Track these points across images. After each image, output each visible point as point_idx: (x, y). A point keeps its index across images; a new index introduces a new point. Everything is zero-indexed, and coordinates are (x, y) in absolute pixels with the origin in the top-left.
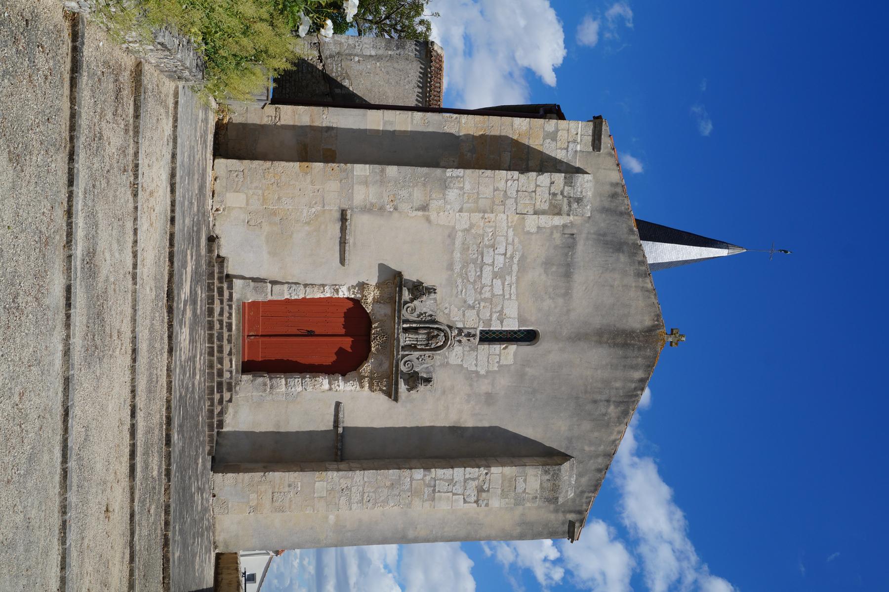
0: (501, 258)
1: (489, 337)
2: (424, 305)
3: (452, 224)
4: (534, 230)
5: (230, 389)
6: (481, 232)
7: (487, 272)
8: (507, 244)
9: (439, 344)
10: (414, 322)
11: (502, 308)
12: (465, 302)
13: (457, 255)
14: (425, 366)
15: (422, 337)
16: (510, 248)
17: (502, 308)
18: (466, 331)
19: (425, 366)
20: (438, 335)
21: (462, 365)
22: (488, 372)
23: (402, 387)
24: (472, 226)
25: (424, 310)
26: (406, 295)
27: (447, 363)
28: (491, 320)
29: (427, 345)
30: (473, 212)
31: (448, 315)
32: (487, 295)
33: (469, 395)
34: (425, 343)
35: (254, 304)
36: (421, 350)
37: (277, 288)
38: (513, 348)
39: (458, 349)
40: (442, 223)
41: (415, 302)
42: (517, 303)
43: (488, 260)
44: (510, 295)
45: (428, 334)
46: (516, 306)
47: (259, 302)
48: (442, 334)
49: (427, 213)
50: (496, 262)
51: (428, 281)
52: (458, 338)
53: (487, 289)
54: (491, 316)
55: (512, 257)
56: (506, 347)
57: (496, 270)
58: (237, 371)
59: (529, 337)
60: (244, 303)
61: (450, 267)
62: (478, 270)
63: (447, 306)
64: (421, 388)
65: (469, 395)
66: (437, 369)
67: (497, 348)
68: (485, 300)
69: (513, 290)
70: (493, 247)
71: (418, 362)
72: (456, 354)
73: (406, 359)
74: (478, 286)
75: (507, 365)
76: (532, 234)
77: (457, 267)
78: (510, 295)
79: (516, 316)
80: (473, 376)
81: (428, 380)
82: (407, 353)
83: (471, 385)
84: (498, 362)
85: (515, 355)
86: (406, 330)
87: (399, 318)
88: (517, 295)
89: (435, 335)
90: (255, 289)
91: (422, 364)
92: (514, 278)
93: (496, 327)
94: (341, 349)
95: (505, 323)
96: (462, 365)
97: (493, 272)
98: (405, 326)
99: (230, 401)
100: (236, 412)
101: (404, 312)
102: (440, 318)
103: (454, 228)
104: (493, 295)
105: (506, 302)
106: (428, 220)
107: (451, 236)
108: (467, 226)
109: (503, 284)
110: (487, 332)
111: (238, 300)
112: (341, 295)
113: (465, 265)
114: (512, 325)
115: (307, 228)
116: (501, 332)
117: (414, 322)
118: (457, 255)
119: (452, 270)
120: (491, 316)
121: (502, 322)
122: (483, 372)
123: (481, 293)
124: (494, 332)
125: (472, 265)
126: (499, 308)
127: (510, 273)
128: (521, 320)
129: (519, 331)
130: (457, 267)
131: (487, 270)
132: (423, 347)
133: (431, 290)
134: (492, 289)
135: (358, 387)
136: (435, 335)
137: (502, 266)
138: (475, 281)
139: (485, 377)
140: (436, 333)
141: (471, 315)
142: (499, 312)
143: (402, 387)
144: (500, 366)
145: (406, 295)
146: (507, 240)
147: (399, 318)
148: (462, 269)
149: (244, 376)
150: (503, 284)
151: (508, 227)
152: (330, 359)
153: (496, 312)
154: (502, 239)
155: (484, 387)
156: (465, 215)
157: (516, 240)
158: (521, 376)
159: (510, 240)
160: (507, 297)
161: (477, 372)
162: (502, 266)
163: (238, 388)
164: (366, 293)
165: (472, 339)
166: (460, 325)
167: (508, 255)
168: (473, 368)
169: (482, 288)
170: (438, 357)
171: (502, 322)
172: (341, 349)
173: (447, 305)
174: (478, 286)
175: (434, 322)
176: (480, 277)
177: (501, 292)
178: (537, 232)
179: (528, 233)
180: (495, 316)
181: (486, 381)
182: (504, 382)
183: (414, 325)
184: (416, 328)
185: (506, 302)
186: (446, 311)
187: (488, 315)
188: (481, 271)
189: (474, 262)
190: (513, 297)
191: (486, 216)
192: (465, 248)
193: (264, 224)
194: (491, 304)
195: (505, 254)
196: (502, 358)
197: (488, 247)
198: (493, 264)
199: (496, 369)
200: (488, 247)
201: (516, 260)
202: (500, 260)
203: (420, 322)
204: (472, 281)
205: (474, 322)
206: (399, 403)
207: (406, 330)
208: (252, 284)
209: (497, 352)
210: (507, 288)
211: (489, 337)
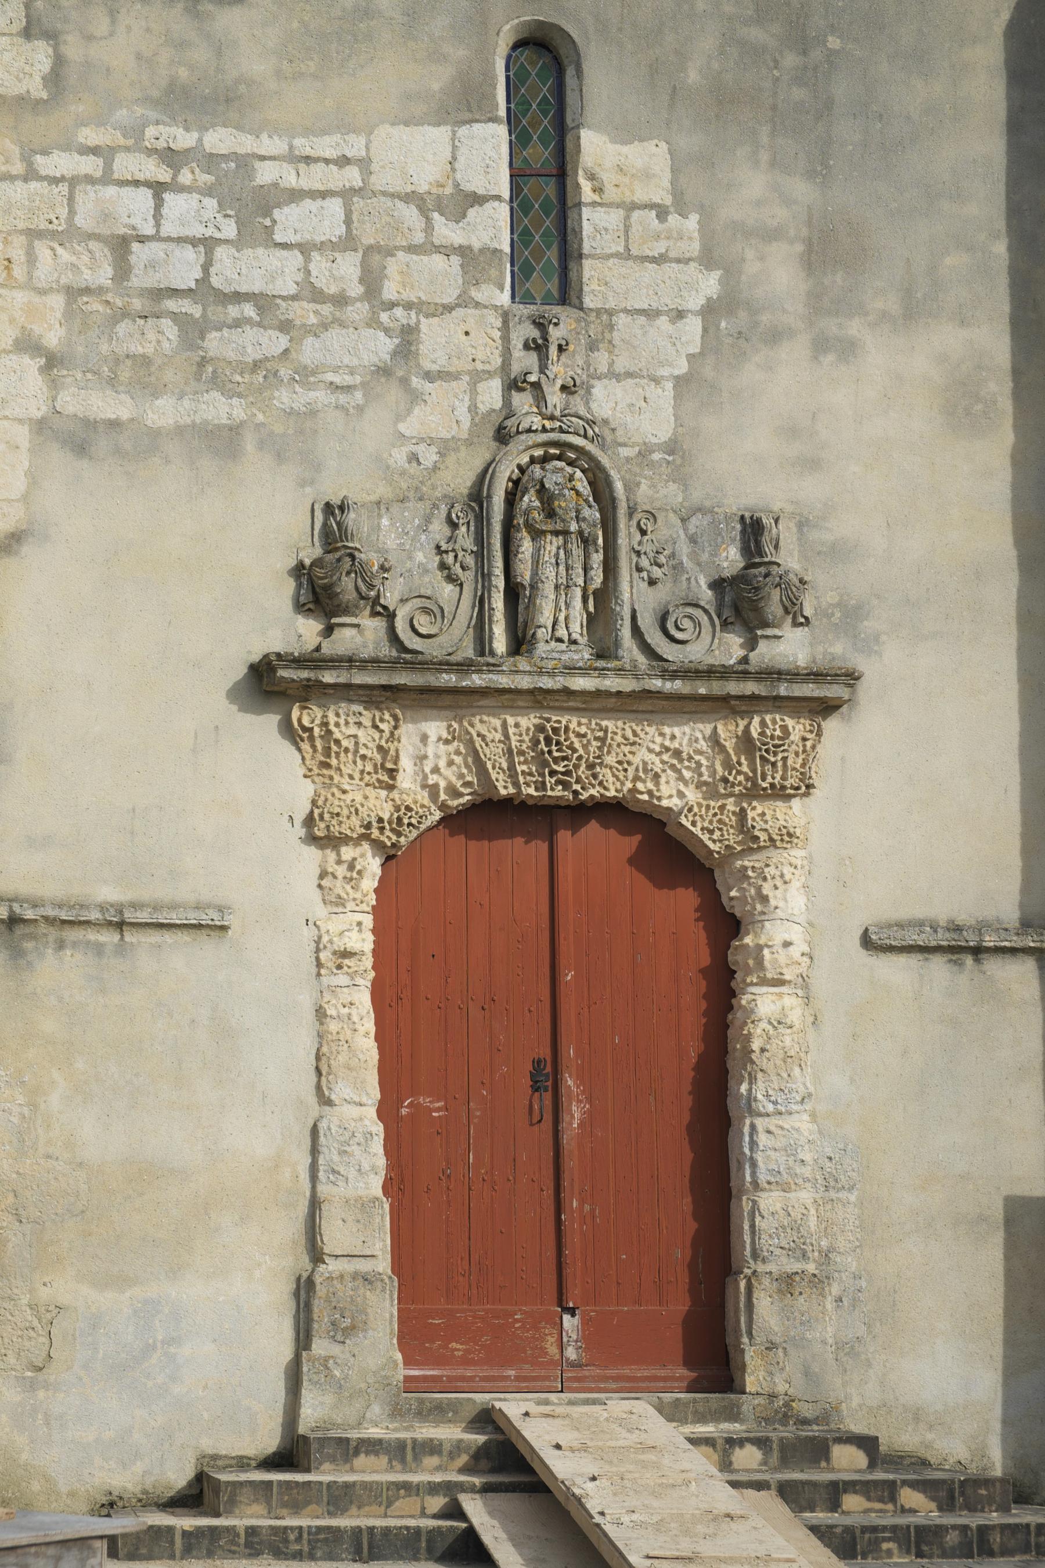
0: (175, 204)
1: (549, 233)
2: (406, 551)
3: (22, 435)
4: (41, 56)
5: (817, 1450)
6: (57, 302)
7: (240, 269)
8: (107, 179)
9: (582, 485)
10: (482, 602)
11: (408, 198)
12: (383, 371)
13: (164, 412)
14: (684, 550)
15: (542, 559)
16: (127, 165)
17: (408, 198)
18: (524, 361)
19: (684, 550)
21: (680, 382)
22: (708, 260)
23: (789, 647)
25: (424, 557)
26: (361, 635)
27: (672, 447)
28: (463, 251)
29: (586, 541)
32: (348, 269)
34: (577, 552)
35: (413, 1336)
36: (610, 567)
37: (336, 1235)
38: (595, 147)
39: (606, 401)
41: (390, 598)
42: (384, 131)
43: (184, 267)
44: (343, 161)
46: (401, 133)
47: (404, 1318)
48: (537, 470)
50: (198, 231)
53: (319, 264)
54: (446, 250)
55: (171, 157)
56: (592, 177)
57: (230, 230)
58: (732, 1414)
59: (545, 59)
60: (857, 679)
61: (223, 442)
62: (233, 311)
63: (407, 444)
64: (789, 558)
65: (821, 345)
66: (697, 495)
67: (597, 225)
68: (371, 282)
69: (327, 146)
70: (121, 246)
71: (668, 577)
72: (631, 410)
74: (305, 313)
75: (674, 171)
76: (59, 61)
77: (218, 408)
78: (343, 161)
79: (442, 133)
80: (733, 323)
81: (753, 532)
84: (662, 213)
85: (626, 132)
86: (521, 641)
87: (465, 667)
88: (346, 128)
89: (539, 496)
90: (345, 1331)
92: (271, 145)
93: (493, 227)
95: (476, 184)
96: (680, 382)
97: (238, 244)
98: (500, 644)
99: (868, 1444)
100: (917, 1415)
102: (459, 478)
103: (40, 426)
104: (348, 242)
105: (378, 182)
107: (79, 438)
108: (32, 365)
109: (295, 195)
111: (396, 1412)
112: (364, 942)
113: (208, 374)
114: (486, 153)
115: (54, 1101)
116: (520, 203)
117: (482, 602)
118: (164, 412)
119: (235, 430)
120: (446, 250)
121: (478, 200)
122: (710, 285)
123: (341, 300)
124: (521, 236)
125: (214, 343)
126: (410, 214)
127: (245, 162)
128: (462, 106)
129: (512, 120)
130: (218, 408)
131: (234, 269)
132: (597, 558)
133: (333, 524)
134: (321, 247)
135: (797, 854)
136: (539, 496)
137: (211, 203)
138: (285, 327)
139: (731, 272)
140: (530, 500)
141: (437, 341)
142: (424, 211)
143: (789, 647)
144: (682, 207)
145: (361, 635)
146: (90, 180)
147: (465, 667)
149: (751, 1383)
150: (295, 195)
151: (31, 174)
153: (429, 228)
154: (87, 200)
155: (779, 276)
157: (90, 136)
158: (722, 102)
159: (90, 165)
160: (352, 176)
161: (710, 311)
162: (211, 203)
163: (807, 1411)
164: (352, 826)
167: (164, 175)
168: (694, 326)
169: (318, 296)
170: (644, 489)
171: (478, 200)
176: (263, 302)
177: (335, 206)
178: (52, 36)
179: (55, 79)
180: (447, 231)
181: (751, 267)
182: (759, 189)
183: (498, 602)
184: (513, 592)
185: (378, 182)
186: (429, 456)
187: (438, 261)
188: (238, 297)
189: (193, 332)
190: (355, 147)
192: (143, 376)
193: (44, 1294)
194: (390, 253)
195: (158, 189)
196: (641, 195)
197: (122, 270)
198: (208, 244)
199: (692, 223)
200: (122, 270)
201: (184, 139)
202: (183, 211)
203: (484, 576)
205: (473, 336)
207: (521, 641)
208: (320, 1346)
209: (612, 219)
210: (315, 177)
211: (549, 233)
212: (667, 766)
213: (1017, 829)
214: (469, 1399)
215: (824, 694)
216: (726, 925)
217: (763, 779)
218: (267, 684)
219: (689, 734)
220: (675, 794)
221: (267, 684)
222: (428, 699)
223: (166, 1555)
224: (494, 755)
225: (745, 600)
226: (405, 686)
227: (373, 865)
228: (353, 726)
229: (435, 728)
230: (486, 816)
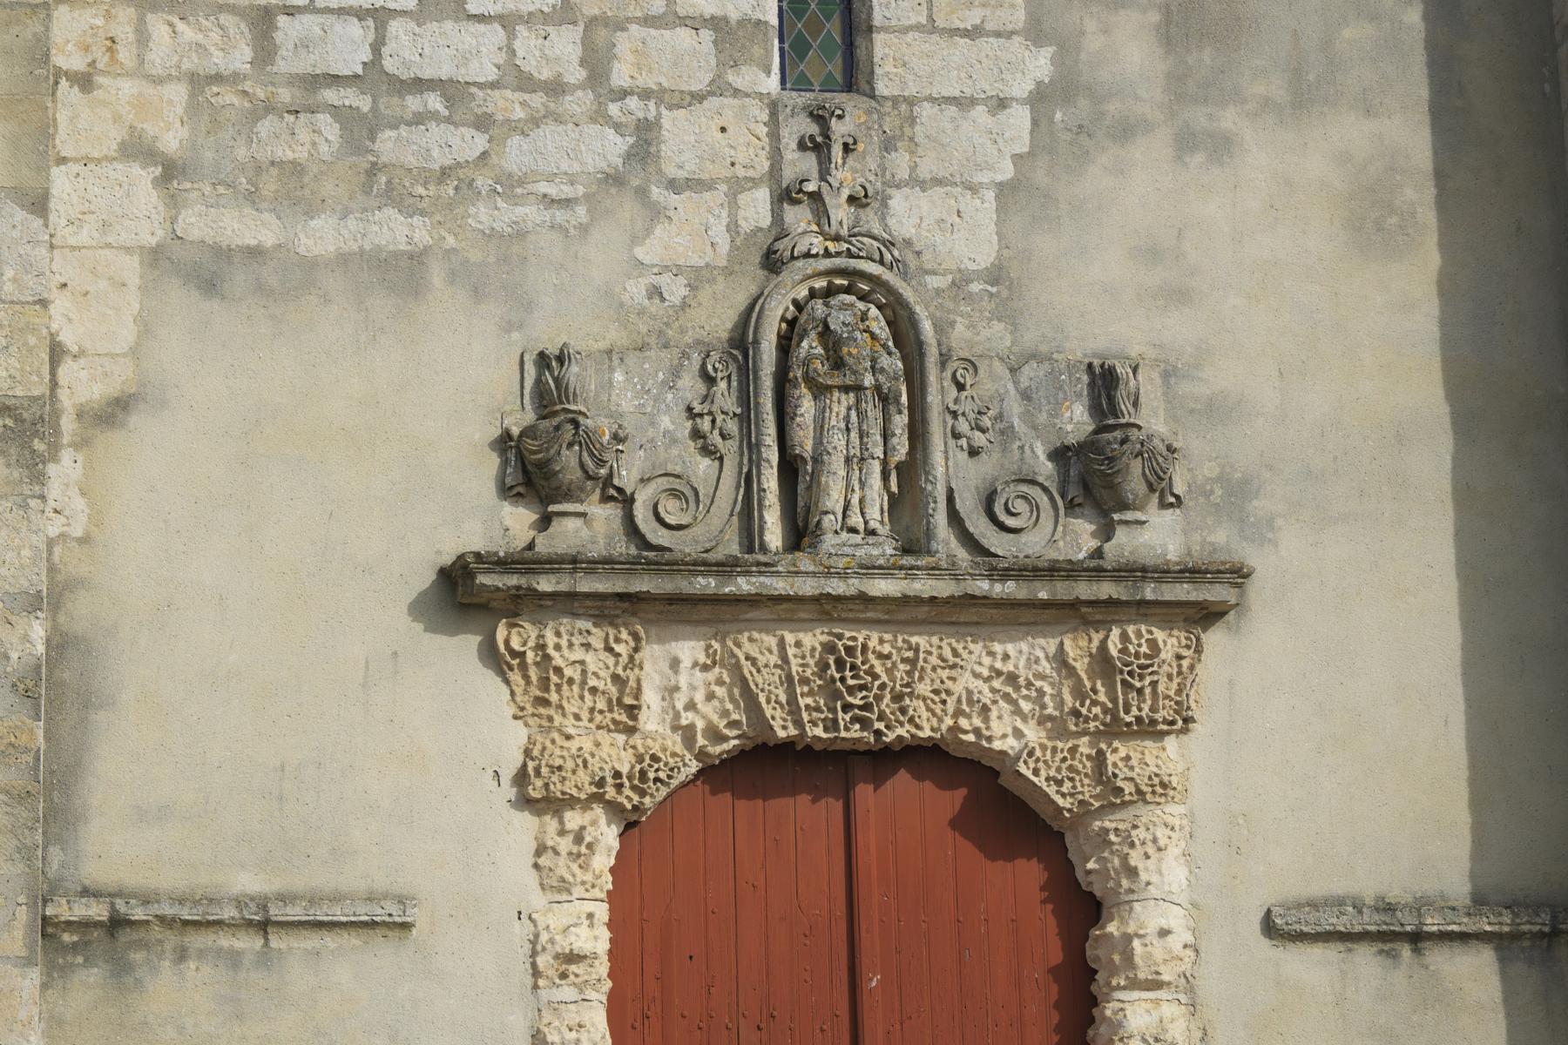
2: (646, 415)
3: (131, 268)
6: (177, 93)
10: (749, 481)
12: (614, 179)
13: (322, 236)
14: (1014, 408)
15: (829, 424)
18: (800, 165)
19: (1014, 408)
20: (825, 332)
22: (1036, 33)
23: (1156, 535)
24: (137, 149)
27: (995, 275)
29: (886, 399)
30: (45, 131)
31: (697, 278)
32: (566, 46)
33: (1186, 142)
34: (874, 413)
36: (918, 432)
39: (907, 215)
40: (127, 334)
41: (626, 478)
45: (820, 391)
49: (68, 424)
51: (494, 395)
52: (841, 213)
53: (527, 43)
61: (402, 274)
62: (413, 103)
64: (1153, 417)
65: (1186, 142)
68: (596, 64)
72: (942, 227)
73: (979, 526)
74: (510, 105)
77: (394, 230)
81: (1104, 384)
82: (940, 518)
83: (1125, 131)
86: (801, 533)
87: (727, 568)
89: (821, 342)
91: (1007, 433)
94: (954, 824)
96: (1005, 191)
98: (774, 536)
101: (683, 545)
103: (155, 256)
106: (113, 413)
107: (207, 272)
108: (143, 176)
110: (794, 49)
113: (379, 185)
117: (749, 481)
118: (322, 236)
119: (418, 258)
122: (1040, 65)
123: (556, 88)
125: (387, 144)
130: (394, 230)
132: (900, 421)
134: (528, 19)
135: (1174, 811)
136: (821, 342)
138: (483, 123)
139: (1066, 50)
140: (810, 345)
141: (685, 140)
143: (1156, 535)
145: (589, 527)
147: (727, 568)
148: (410, 209)
152: (1030, 873)
156: (61, 182)
161: (1040, 99)
165: (839, 129)
166: (757, 208)
168: (1020, 117)
169: (526, 83)
172: (954, 824)
173: (636, 291)
174: (510, 105)
175: (742, 342)
181: (1093, 42)
183: (770, 481)
184: (790, 467)
186: (676, 290)
187: (684, 36)
188: (420, 85)
191: (69, 59)
192: (293, 188)
197: (265, 51)
200: (265, 51)
204: (480, 142)
206: (1251, 556)
207: (801, 533)
212: (997, 695)
215: (1203, 599)
216: (1083, 909)
217: (1128, 710)
218: (464, 594)
219: (1026, 653)
220: (1009, 733)
221: (464, 594)
224: (768, 685)
225: (1097, 473)
226: (650, 595)
227: (608, 836)
228: (580, 649)
229: (689, 650)
230: (759, 766)
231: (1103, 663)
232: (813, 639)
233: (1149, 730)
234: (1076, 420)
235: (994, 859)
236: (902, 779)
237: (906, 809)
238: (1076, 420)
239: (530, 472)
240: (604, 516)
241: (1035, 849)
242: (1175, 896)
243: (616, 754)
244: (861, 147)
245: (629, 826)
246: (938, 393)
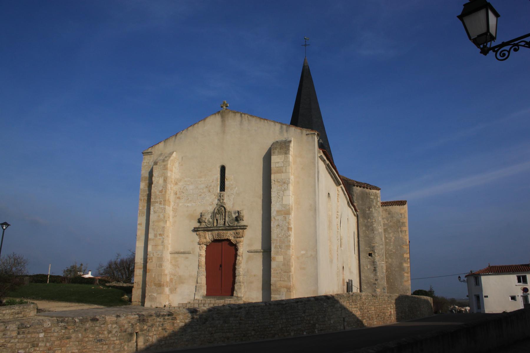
23: (242, 223)
152: (234, 247)
212: (230, 235)
213: (494, 312)
214: (417, 298)
215: (244, 228)
216: (236, 250)
217: (237, 236)
218: (195, 230)
219: (232, 232)
220: (232, 238)
221: (195, 230)
222: (208, 231)
223: (339, 305)
224: (214, 235)
225: (237, 219)
226: (206, 229)
227: (205, 246)
228: (201, 233)
229: (210, 233)
230: (215, 241)
231: (237, 233)
232: (217, 232)
233: (240, 237)
234: (237, 215)
235: (504, 312)
236: (223, 242)
237: (225, 244)
238: (237, 215)
239: (199, 221)
240: (204, 224)
241: (234, 247)
242: (242, 249)
243: (205, 241)
244: (370, 257)
245: (207, 246)
246: (227, 214)
